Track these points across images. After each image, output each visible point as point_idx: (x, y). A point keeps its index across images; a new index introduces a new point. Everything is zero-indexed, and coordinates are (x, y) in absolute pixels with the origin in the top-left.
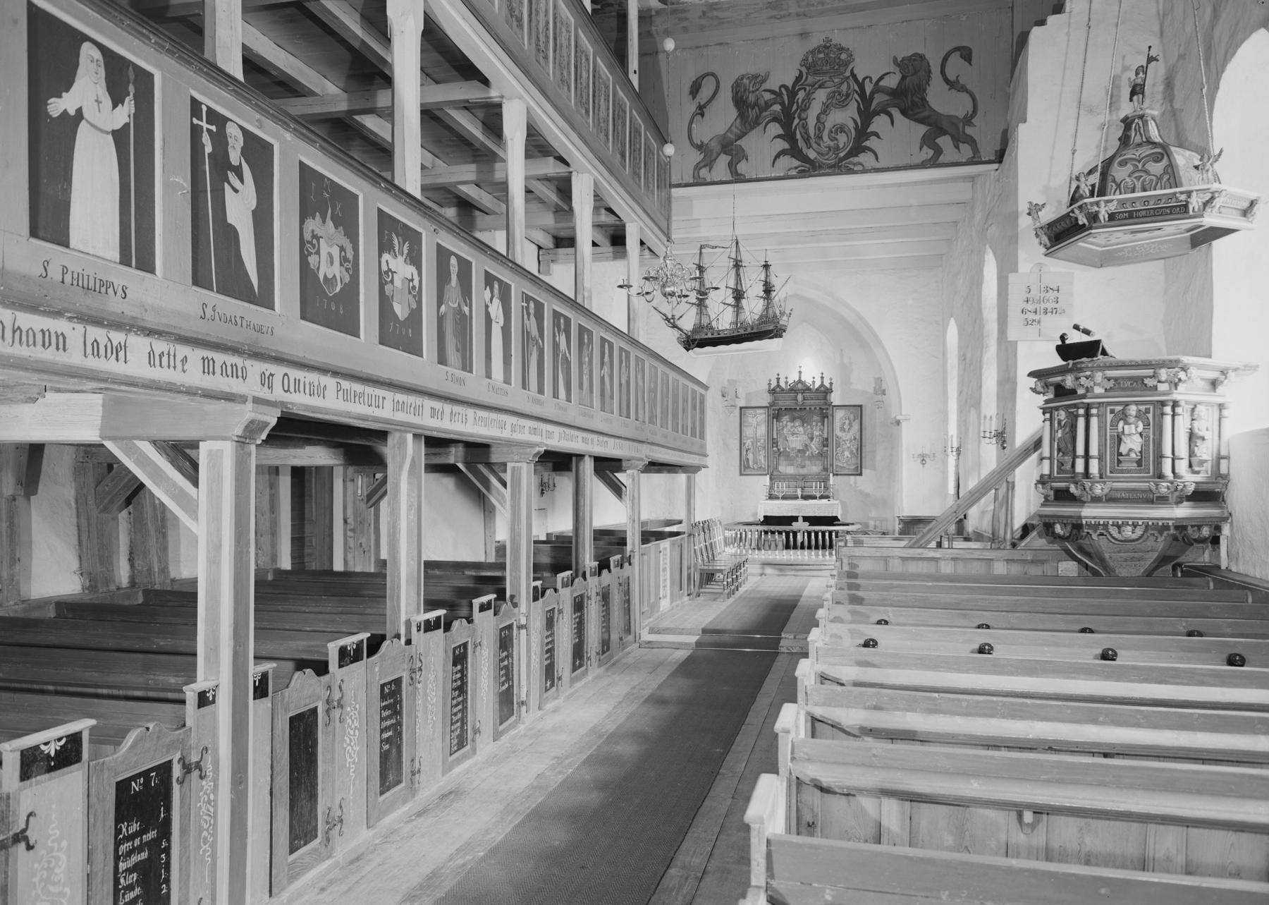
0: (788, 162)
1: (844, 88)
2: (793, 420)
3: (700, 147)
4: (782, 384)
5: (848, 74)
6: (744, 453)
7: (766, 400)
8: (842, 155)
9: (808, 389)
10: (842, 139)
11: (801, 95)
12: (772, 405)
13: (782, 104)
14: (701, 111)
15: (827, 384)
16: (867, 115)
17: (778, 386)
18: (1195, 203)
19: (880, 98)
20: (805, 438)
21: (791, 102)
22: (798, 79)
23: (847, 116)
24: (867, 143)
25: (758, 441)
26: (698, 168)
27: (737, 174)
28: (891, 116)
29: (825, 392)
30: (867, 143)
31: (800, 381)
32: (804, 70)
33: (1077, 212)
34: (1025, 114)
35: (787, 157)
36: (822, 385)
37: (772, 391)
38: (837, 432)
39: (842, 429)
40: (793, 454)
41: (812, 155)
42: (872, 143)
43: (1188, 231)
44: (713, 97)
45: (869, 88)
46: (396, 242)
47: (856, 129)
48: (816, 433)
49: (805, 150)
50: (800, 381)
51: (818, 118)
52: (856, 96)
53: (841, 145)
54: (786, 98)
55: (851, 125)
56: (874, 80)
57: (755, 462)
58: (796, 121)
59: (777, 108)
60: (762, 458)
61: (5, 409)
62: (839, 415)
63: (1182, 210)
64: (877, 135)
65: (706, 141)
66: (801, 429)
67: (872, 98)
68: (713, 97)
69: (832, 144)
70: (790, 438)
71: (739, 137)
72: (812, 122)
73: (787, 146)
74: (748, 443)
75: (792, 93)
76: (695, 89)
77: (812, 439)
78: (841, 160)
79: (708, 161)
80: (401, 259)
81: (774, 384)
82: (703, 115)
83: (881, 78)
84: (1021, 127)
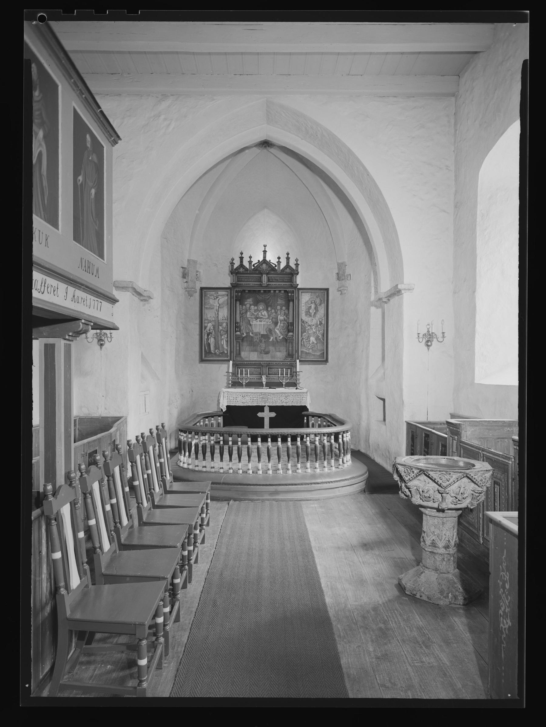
2: (256, 303)
7: (226, 281)
9: (273, 269)
12: (234, 286)
15: (292, 264)
17: (242, 265)
25: (220, 324)
31: (264, 260)
36: (288, 266)
37: (234, 272)
38: (303, 316)
50: (264, 260)
60: (224, 343)
62: (305, 298)
74: (210, 325)
81: (237, 264)
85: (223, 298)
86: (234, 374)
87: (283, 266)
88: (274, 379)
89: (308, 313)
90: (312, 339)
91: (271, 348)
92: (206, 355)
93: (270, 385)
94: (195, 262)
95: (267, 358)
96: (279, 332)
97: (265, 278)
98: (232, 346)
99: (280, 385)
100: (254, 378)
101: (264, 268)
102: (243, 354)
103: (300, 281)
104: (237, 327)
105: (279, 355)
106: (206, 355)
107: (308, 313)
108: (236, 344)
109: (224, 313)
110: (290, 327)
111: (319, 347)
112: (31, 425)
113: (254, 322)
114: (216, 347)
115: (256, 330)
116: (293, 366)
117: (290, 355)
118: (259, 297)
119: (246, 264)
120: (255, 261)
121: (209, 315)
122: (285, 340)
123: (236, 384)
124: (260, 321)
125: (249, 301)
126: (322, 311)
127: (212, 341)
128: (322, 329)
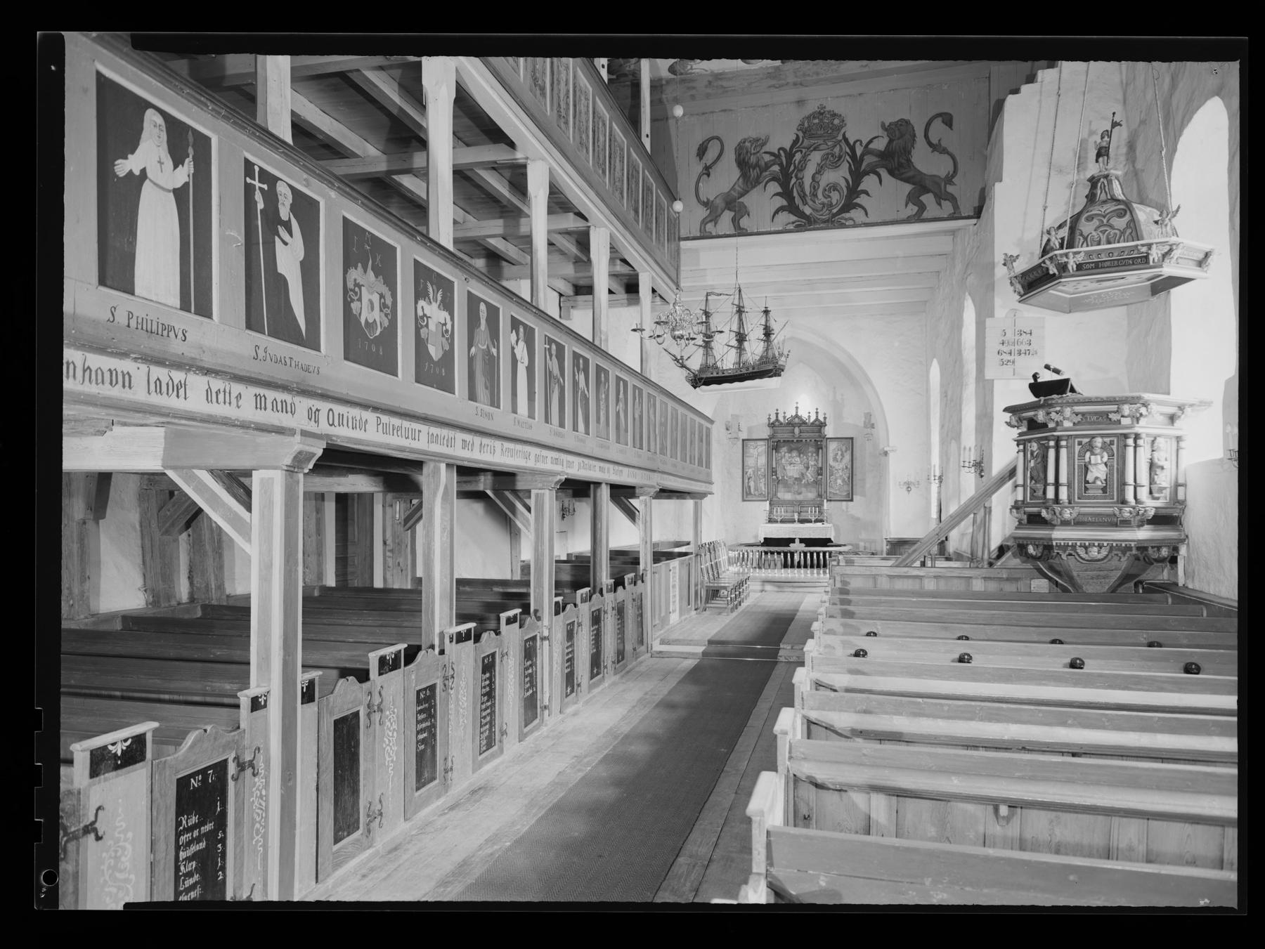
0: (786, 218)
1: (837, 150)
2: (790, 451)
3: (706, 204)
5: (840, 137)
7: (766, 433)
9: (804, 423)
11: (798, 156)
12: (772, 437)
13: (781, 165)
14: (707, 171)
15: (821, 418)
16: (857, 175)
17: (777, 420)
18: (1155, 254)
19: (869, 159)
20: (801, 467)
21: (789, 164)
22: (795, 142)
23: (839, 176)
24: (857, 201)
25: (758, 470)
26: (704, 222)
27: (740, 228)
30: (857, 201)
31: (797, 416)
32: (801, 134)
33: (1048, 262)
36: (817, 419)
37: (772, 425)
38: (831, 462)
40: (790, 482)
41: (808, 211)
42: (862, 200)
45: (859, 151)
47: (848, 187)
49: (801, 207)
50: (797, 416)
55: (843, 184)
58: (793, 180)
59: (776, 168)
60: (762, 485)
62: (832, 446)
63: (1144, 260)
69: (826, 201)
71: (742, 195)
72: (807, 182)
74: (750, 471)
75: (790, 155)
76: (702, 151)
78: (834, 215)
81: (773, 418)
83: (871, 141)
84: (998, 186)
85: (762, 447)
86: (771, 512)
87: (812, 419)
88: (804, 516)
89: (835, 459)
90: (839, 481)
91: (804, 489)
92: (747, 495)
93: (802, 521)
94: (737, 416)
95: (800, 498)
96: (810, 476)
97: (797, 430)
98: (637, 431)
99: (810, 521)
100: (788, 516)
101: (796, 423)
102: (779, 495)
103: (829, 431)
104: (774, 472)
105: (810, 495)
106: (747, 495)
107: (835, 459)
108: (448, 356)
109: (762, 460)
110: (820, 472)
111: (846, 488)
112: (692, 58)
113: (788, 467)
114: (756, 489)
115: (790, 474)
116: (820, 506)
117: (820, 496)
118: (793, 446)
119: (781, 419)
120: (788, 416)
121: (750, 462)
122: (816, 482)
123: (771, 521)
124: (793, 465)
125: (784, 449)
126: (848, 457)
127: (752, 484)
128: (847, 473)
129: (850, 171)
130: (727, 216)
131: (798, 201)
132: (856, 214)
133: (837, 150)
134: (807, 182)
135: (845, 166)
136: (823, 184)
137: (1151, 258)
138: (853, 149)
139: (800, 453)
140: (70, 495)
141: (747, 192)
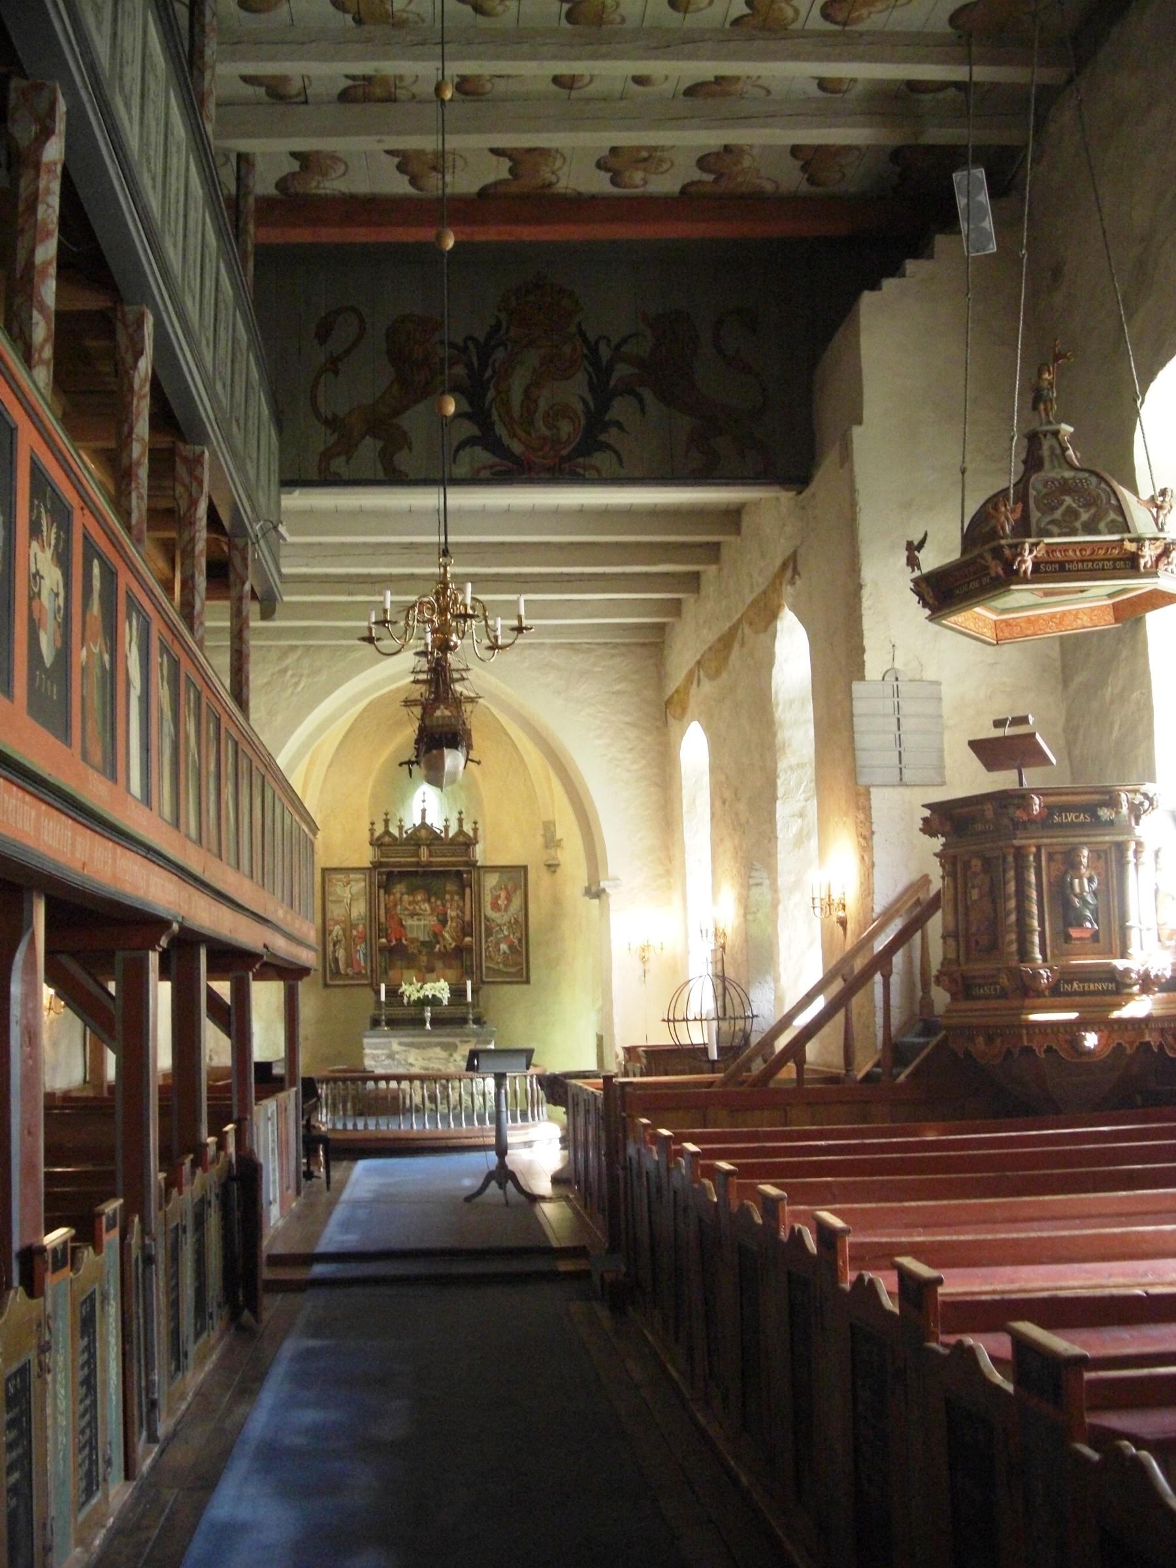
0: (482, 456)
1: (567, 349)
2: (412, 891)
3: (332, 423)
4: (394, 831)
5: (573, 329)
6: (330, 948)
7: (365, 856)
8: (564, 452)
9: (437, 837)
10: (566, 428)
11: (500, 354)
12: (376, 865)
13: (468, 366)
14: (333, 364)
15: (468, 828)
16: (602, 393)
17: (387, 832)
18: (1149, 553)
19: (622, 370)
20: (433, 921)
21: (484, 365)
22: (496, 328)
23: (574, 391)
24: (603, 437)
25: (354, 926)
26: (327, 455)
27: (394, 471)
28: (641, 401)
29: (465, 843)
30: (603, 437)
31: (423, 825)
32: (503, 316)
33: (989, 557)
34: (860, 408)
35: (478, 450)
36: (461, 832)
37: (376, 843)
38: (488, 911)
39: (495, 906)
40: (412, 949)
41: (517, 447)
42: (611, 436)
43: (1110, 596)
44: (355, 344)
45: (605, 352)
46: (44, 522)
47: (588, 411)
48: (452, 913)
49: (506, 440)
50: (423, 825)
51: (527, 392)
52: (586, 363)
53: (564, 435)
54: (475, 359)
55: (579, 407)
56: (614, 342)
57: (349, 963)
58: (491, 394)
59: (460, 370)
60: (360, 957)
61: (1173, 1012)
62: (491, 881)
63: (1129, 564)
64: (619, 425)
65: (341, 415)
66: (426, 906)
67: (609, 370)
68: (355, 344)
69: (548, 433)
70: (409, 922)
71: (396, 413)
72: (517, 397)
73: (478, 433)
74: (337, 930)
75: (485, 352)
76: (324, 332)
77: (443, 922)
78: (564, 460)
79: (346, 446)
80: (49, 553)
81: (379, 830)
82: (336, 373)
83: (624, 341)
84: (857, 431)
85: (359, 885)
98: (287, 878)
110: (466, 929)
129: (592, 389)
130: (369, 448)
131: (500, 430)
132: (600, 459)
133: (567, 349)
134: (517, 397)
135: (581, 377)
136: (543, 405)
137: (1142, 562)
138: (594, 350)
139: (430, 894)
140: (47, 384)
141: (406, 408)
